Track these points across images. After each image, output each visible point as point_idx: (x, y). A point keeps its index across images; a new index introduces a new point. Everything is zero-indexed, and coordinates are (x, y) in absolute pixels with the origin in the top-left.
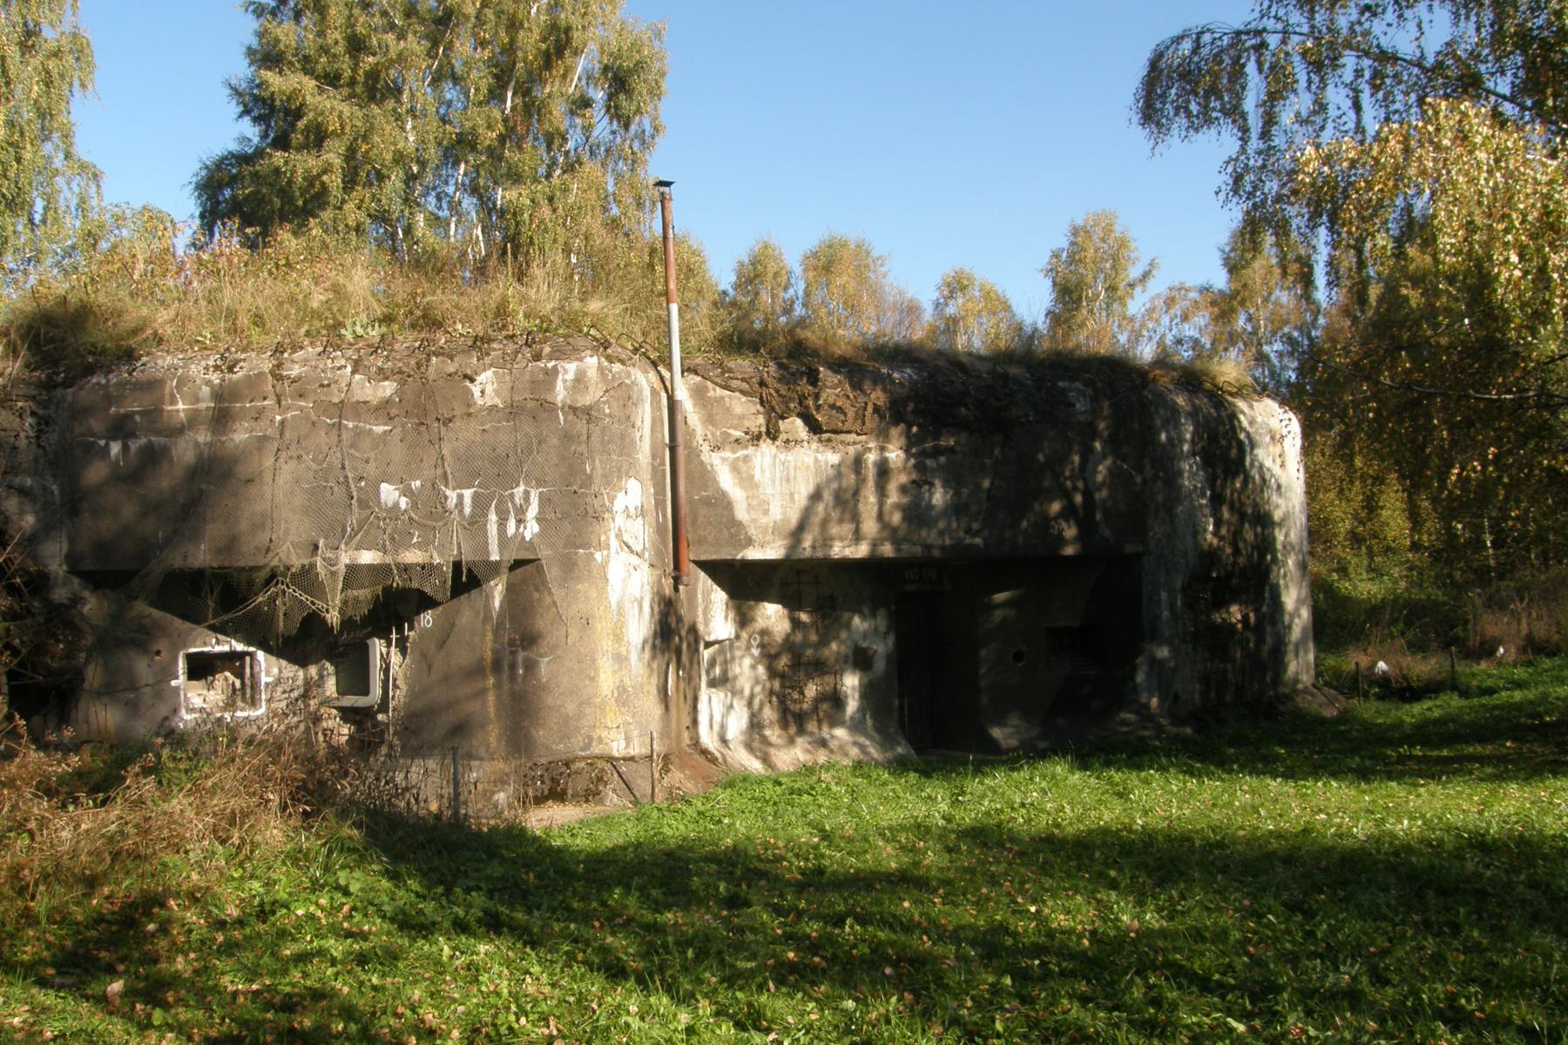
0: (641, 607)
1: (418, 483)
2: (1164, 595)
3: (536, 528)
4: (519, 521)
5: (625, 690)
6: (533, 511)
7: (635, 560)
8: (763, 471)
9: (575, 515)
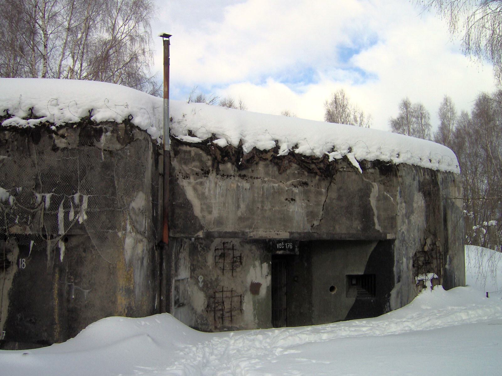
0: (142, 263)
1: (21, 189)
2: (405, 260)
3: (85, 217)
4: (76, 213)
5: (132, 309)
6: (85, 205)
7: (139, 237)
8: (209, 190)
9: (108, 210)
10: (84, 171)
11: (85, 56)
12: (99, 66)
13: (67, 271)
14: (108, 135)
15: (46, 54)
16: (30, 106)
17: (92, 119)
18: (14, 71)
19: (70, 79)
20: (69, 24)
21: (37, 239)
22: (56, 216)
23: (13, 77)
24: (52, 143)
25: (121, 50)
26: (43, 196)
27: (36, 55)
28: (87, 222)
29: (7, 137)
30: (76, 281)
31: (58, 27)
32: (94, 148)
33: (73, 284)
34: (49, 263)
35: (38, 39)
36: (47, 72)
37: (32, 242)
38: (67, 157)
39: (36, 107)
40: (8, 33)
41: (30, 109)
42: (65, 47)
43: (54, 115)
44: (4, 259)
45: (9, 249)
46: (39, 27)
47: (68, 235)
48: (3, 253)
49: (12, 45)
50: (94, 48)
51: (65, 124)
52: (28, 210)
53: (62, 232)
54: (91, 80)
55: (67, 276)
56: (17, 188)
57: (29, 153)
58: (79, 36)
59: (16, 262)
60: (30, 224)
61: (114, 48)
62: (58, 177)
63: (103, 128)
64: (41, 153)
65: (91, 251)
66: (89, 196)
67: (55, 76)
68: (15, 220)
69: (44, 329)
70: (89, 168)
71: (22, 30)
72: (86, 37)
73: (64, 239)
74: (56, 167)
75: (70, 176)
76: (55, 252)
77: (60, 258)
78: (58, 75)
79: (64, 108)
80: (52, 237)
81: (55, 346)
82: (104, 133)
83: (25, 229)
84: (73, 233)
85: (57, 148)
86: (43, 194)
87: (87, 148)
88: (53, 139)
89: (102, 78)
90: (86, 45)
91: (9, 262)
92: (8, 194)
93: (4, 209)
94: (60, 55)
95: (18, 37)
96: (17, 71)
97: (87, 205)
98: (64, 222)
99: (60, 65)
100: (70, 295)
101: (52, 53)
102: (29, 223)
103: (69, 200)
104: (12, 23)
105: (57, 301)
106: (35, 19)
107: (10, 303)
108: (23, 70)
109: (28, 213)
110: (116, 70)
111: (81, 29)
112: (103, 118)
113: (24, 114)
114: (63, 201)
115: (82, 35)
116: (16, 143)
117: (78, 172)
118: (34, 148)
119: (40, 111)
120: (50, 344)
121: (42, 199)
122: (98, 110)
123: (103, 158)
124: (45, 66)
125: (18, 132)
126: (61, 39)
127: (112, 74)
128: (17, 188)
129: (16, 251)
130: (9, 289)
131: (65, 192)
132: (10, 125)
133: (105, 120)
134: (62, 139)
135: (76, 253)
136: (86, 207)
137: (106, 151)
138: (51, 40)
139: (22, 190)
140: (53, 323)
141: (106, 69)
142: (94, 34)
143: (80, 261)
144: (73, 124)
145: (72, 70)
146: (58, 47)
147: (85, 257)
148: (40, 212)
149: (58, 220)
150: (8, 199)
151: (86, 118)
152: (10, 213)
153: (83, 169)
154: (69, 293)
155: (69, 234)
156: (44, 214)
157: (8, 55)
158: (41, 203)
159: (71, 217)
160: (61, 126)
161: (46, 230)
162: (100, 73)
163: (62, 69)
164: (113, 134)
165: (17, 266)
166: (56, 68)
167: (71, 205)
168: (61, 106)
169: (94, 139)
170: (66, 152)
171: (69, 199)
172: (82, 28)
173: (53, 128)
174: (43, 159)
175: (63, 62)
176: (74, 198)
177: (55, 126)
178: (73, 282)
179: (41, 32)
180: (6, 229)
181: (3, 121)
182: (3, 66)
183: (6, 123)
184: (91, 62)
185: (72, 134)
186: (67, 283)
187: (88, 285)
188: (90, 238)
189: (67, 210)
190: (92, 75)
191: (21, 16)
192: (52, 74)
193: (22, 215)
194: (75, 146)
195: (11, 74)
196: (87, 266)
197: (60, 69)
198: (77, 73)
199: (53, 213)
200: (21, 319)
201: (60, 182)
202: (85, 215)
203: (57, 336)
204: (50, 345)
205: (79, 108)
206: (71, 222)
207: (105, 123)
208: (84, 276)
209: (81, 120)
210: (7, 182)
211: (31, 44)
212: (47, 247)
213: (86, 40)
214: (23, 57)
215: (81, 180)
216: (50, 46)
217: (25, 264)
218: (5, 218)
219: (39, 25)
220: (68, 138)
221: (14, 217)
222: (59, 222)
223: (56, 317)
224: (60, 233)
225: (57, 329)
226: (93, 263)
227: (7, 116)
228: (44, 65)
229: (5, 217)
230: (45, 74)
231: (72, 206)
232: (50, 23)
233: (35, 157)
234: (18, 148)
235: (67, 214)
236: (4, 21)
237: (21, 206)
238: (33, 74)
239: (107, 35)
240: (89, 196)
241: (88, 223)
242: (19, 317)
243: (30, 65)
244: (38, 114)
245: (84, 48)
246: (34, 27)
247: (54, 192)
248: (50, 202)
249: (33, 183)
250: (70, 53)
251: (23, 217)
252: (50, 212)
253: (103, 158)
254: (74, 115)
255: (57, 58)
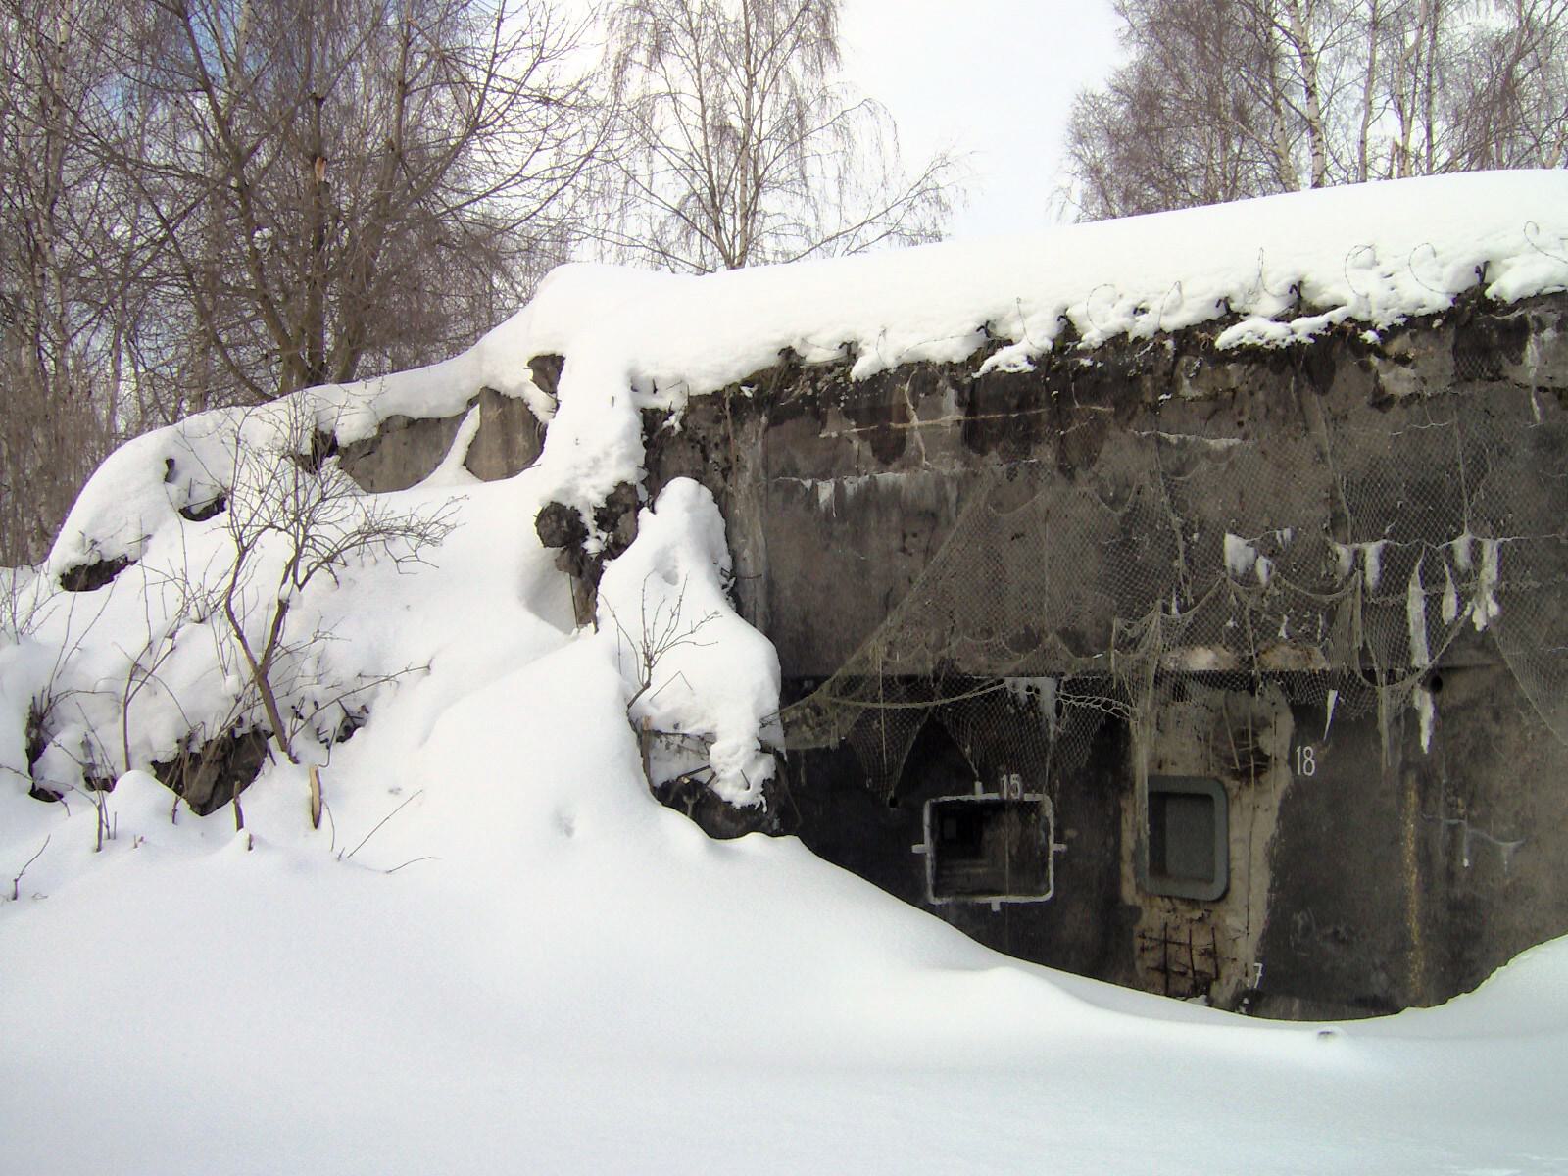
1: (1287, 533)
3: (1494, 609)
4: (1463, 598)
6: (1490, 572)
10: (1478, 462)
11: (1436, 101)
12: (1487, 121)
13: (1444, 781)
14: (1546, 340)
15: (1316, 114)
16: (1294, 280)
17: (1489, 293)
18: (1228, 182)
19: (1400, 177)
20: (1373, 9)
21: (1346, 684)
22: (1402, 610)
23: (1227, 200)
24: (1372, 385)
25: (1554, 57)
26: (1357, 552)
27: (1285, 123)
28: (1498, 625)
29: (1234, 382)
30: (1474, 814)
31: (1340, 25)
32: (1503, 386)
33: (1465, 823)
34: (1388, 758)
35: (1284, 74)
36: (1326, 169)
37: (1332, 695)
38: (1421, 425)
39: (1311, 279)
40: (1195, 70)
41: (1294, 287)
42: (1370, 81)
43: (1367, 297)
44: (1251, 748)
45: (1263, 718)
46: (1284, 37)
47: (1441, 670)
48: (1247, 730)
49: (1213, 107)
50: (1461, 68)
51: (1405, 319)
52: (1313, 596)
53: (1422, 659)
54: (1468, 169)
55: (1446, 798)
56: (1278, 533)
57: (1305, 421)
58: (1411, 38)
59: (1286, 757)
60: (1323, 639)
61: (1529, 57)
62: (1398, 489)
63: (1529, 316)
64: (1338, 419)
65: (1519, 717)
66: (1501, 540)
67: (1351, 179)
68: (1279, 629)
69: (1377, 962)
70: (1495, 450)
71: (1236, 56)
72: (1434, 38)
73: (1429, 682)
74: (1390, 456)
75: (1435, 482)
76: (1403, 723)
77: (1420, 741)
78: (1362, 171)
79: (1398, 271)
80: (1391, 677)
81: (1410, 1014)
82: (1533, 335)
83: (1309, 656)
84: (1457, 663)
85: (1387, 400)
86: (1357, 545)
87: (1483, 390)
88: (1374, 371)
89: (1500, 161)
90: (1436, 65)
91: (1266, 759)
92: (1251, 551)
93: (1243, 597)
94: (1358, 110)
95: (1225, 80)
96: (1235, 180)
97: (1496, 571)
98: (1428, 628)
99: (1362, 142)
100: (1455, 860)
101: (1332, 109)
102: (1319, 637)
103: (1437, 558)
104: (1203, 40)
105: (1414, 877)
106: (1267, 14)
107: (1273, 880)
108: (1252, 174)
109: (1313, 607)
110: (1544, 125)
111: (1413, 16)
112: (1524, 287)
113: (1275, 306)
114: (1420, 562)
115: (1421, 35)
116: (1261, 396)
117: (1462, 469)
118: (1316, 403)
119: (1324, 289)
120: (1396, 1010)
121: (1356, 560)
122: (1506, 261)
123: (1538, 417)
124: (1317, 154)
125: (1264, 362)
126: (1354, 60)
127: (1530, 142)
128: (1278, 533)
129: (1286, 723)
130: (1268, 838)
131: (1423, 535)
132: (1238, 342)
133: (1532, 292)
134: (1401, 367)
135: (1470, 725)
136: (1495, 577)
137: (1546, 390)
138: (1326, 70)
139: (1292, 538)
140: (1402, 944)
141: (1510, 126)
142: (1456, 23)
143: (1484, 751)
144: (1430, 317)
145: (1401, 152)
146: (1348, 88)
147: (1500, 737)
148: (1350, 600)
149: (1408, 625)
150: (1254, 566)
151: (1470, 293)
152: (1261, 611)
153: (1474, 458)
154: (1452, 852)
155: (1447, 663)
156: (1364, 606)
157: (1204, 139)
158: (1351, 575)
159: (1447, 610)
160: (1392, 327)
161: (1373, 655)
162: (1494, 146)
163: (1369, 153)
164: (1562, 333)
165: (1288, 768)
166: (1350, 155)
167: (1444, 575)
168: (1386, 267)
169: (1503, 357)
170: (1415, 407)
171: (1438, 554)
172: (1416, 12)
173: (1370, 336)
174: (1346, 436)
175: (1370, 132)
176: (1452, 552)
177: (1374, 330)
178: (1461, 818)
179: (1293, 50)
180: (1251, 658)
181: (1216, 334)
182: (1195, 172)
183: (1226, 338)
184: (1457, 115)
185: (1430, 349)
186: (1444, 821)
187: (1513, 826)
188: (1512, 676)
189: (1434, 591)
190: (1467, 156)
191: (1226, 16)
192: (1342, 174)
193: (1296, 615)
194: (1442, 386)
195: (1220, 193)
196: (1506, 765)
197: (1363, 154)
198: (1418, 157)
199: (1391, 601)
200: (1307, 929)
201: (1408, 504)
202: (1492, 601)
203: (1418, 984)
204: (1396, 1011)
205: (1443, 265)
206: (1450, 628)
207: (1533, 302)
208: (1499, 796)
209: (1454, 300)
210: (1247, 517)
211: (1266, 94)
212: (1376, 706)
213: (1433, 47)
214: (1249, 137)
215: (1473, 492)
216: (1323, 86)
217: (1313, 763)
218: (1249, 626)
219: (1284, 32)
220: (1419, 362)
221: (1273, 621)
222: (1412, 628)
223: (1414, 925)
224: (1415, 662)
225: (1417, 963)
226: (1528, 756)
227: (1228, 317)
228: (1315, 151)
229: (1248, 621)
230: (1321, 176)
231: (1448, 575)
232: (1317, 17)
233: (1322, 432)
234: (1268, 410)
235: (1433, 603)
236: (1180, 41)
237: (1292, 587)
238: (1283, 180)
239: (1501, 16)
240: (1501, 540)
241: (1503, 629)
242: (1301, 923)
243: (1271, 157)
244: (1318, 301)
245: (1430, 76)
246: (1268, 40)
247: (1391, 536)
248: (1378, 569)
249: (1323, 512)
250: (1388, 97)
251: (1301, 618)
252: (1382, 598)
253: (1538, 417)
254: (1431, 290)
255: (1351, 122)
